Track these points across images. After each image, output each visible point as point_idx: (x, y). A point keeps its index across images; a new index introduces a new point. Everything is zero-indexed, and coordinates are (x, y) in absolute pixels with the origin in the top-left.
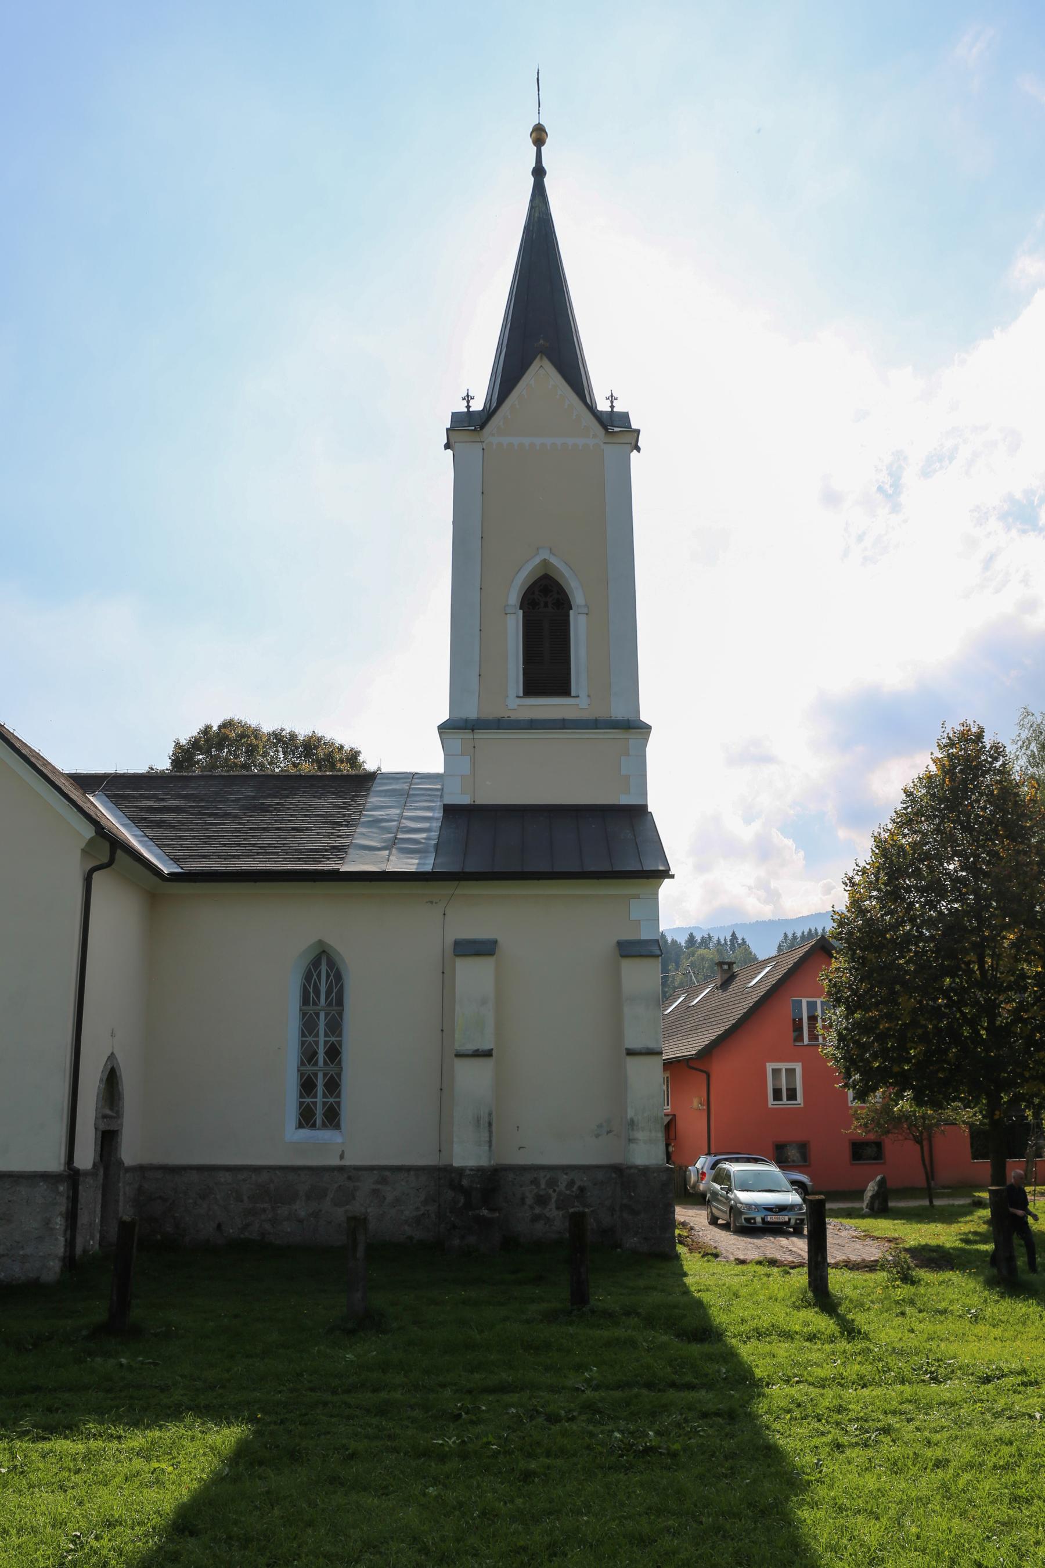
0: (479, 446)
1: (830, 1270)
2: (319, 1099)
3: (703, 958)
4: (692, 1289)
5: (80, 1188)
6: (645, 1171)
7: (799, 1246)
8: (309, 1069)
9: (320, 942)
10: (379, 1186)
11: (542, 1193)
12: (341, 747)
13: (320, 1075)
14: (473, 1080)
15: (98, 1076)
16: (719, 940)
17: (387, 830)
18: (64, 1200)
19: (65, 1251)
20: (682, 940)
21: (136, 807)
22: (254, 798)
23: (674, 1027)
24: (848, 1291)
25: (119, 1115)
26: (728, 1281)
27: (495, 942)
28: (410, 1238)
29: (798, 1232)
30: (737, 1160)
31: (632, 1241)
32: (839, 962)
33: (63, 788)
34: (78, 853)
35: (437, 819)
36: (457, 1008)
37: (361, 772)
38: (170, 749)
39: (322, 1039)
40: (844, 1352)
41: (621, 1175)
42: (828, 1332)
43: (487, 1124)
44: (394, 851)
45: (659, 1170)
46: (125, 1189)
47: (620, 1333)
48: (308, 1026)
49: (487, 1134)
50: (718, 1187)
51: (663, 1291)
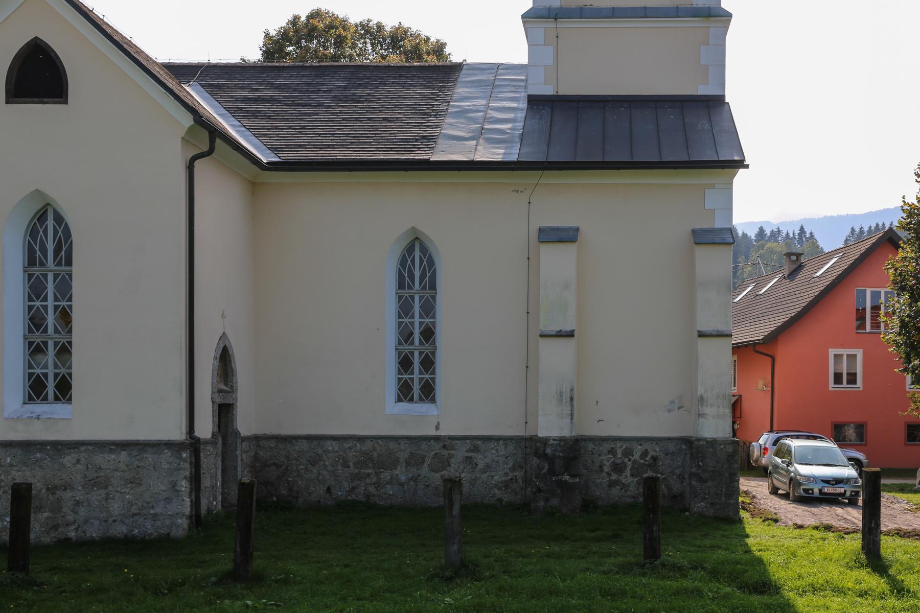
1: (882, 537)
2: (416, 376)
3: (772, 251)
4: (754, 548)
5: (202, 454)
6: (713, 443)
7: (855, 516)
8: (406, 348)
9: (413, 229)
10: (470, 454)
11: (618, 461)
12: (427, 39)
13: (416, 354)
14: (556, 358)
15: (213, 353)
16: (788, 234)
17: (474, 120)
18: (187, 466)
19: (191, 510)
20: (752, 234)
21: (232, 97)
22: (345, 88)
23: (743, 313)
24: (899, 555)
25: (233, 390)
26: (787, 543)
27: (577, 230)
28: (500, 500)
29: (852, 503)
30: (798, 437)
31: (699, 506)
32: (907, 252)
33: (158, 75)
34: (178, 143)
35: (522, 110)
37: (448, 63)
38: (260, 40)
39: (417, 320)
40: (893, 607)
41: (691, 447)
42: (879, 590)
43: (570, 400)
44: (481, 141)
45: (725, 442)
46: (243, 457)
47: (687, 583)
48: (404, 308)
49: (569, 408)
50: (779, 460)
51: (726, 549)
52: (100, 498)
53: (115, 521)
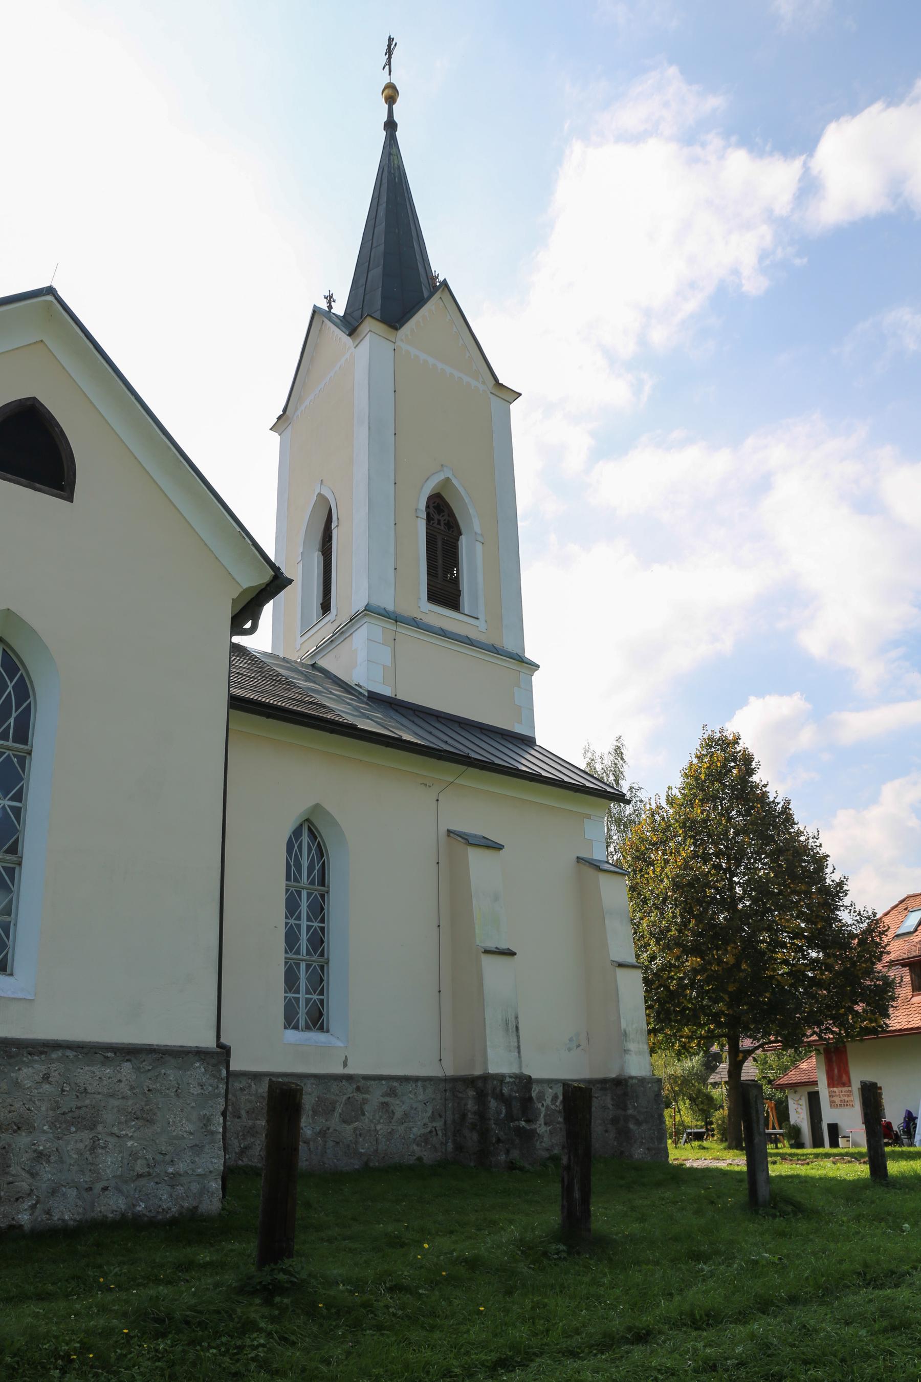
0: (392, 346)
10: (387, 1099)
28: (420, 1159)
36: (474, 900)
49: (515, 1040)
52: (81, 1146)
53: (105, 1189)
